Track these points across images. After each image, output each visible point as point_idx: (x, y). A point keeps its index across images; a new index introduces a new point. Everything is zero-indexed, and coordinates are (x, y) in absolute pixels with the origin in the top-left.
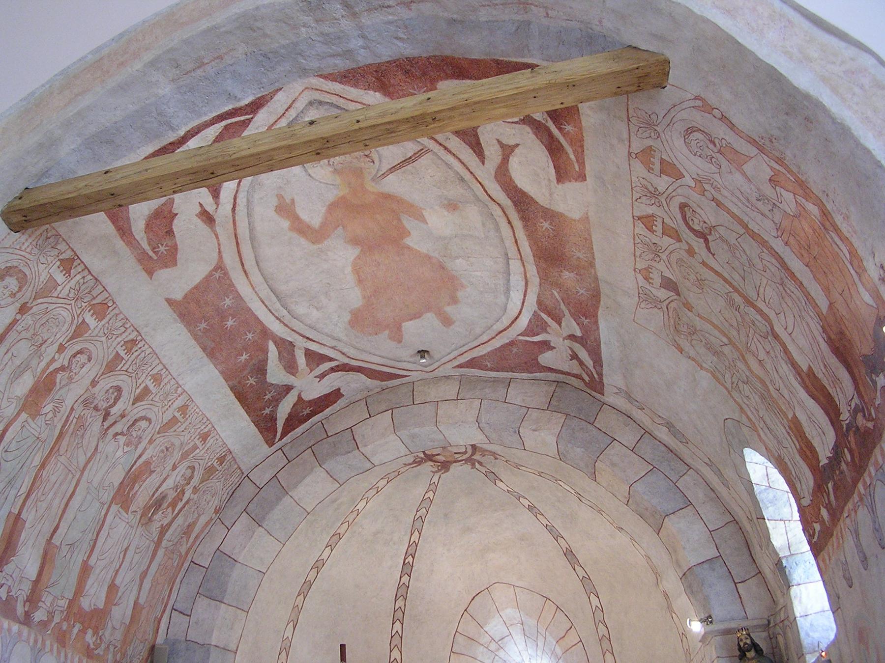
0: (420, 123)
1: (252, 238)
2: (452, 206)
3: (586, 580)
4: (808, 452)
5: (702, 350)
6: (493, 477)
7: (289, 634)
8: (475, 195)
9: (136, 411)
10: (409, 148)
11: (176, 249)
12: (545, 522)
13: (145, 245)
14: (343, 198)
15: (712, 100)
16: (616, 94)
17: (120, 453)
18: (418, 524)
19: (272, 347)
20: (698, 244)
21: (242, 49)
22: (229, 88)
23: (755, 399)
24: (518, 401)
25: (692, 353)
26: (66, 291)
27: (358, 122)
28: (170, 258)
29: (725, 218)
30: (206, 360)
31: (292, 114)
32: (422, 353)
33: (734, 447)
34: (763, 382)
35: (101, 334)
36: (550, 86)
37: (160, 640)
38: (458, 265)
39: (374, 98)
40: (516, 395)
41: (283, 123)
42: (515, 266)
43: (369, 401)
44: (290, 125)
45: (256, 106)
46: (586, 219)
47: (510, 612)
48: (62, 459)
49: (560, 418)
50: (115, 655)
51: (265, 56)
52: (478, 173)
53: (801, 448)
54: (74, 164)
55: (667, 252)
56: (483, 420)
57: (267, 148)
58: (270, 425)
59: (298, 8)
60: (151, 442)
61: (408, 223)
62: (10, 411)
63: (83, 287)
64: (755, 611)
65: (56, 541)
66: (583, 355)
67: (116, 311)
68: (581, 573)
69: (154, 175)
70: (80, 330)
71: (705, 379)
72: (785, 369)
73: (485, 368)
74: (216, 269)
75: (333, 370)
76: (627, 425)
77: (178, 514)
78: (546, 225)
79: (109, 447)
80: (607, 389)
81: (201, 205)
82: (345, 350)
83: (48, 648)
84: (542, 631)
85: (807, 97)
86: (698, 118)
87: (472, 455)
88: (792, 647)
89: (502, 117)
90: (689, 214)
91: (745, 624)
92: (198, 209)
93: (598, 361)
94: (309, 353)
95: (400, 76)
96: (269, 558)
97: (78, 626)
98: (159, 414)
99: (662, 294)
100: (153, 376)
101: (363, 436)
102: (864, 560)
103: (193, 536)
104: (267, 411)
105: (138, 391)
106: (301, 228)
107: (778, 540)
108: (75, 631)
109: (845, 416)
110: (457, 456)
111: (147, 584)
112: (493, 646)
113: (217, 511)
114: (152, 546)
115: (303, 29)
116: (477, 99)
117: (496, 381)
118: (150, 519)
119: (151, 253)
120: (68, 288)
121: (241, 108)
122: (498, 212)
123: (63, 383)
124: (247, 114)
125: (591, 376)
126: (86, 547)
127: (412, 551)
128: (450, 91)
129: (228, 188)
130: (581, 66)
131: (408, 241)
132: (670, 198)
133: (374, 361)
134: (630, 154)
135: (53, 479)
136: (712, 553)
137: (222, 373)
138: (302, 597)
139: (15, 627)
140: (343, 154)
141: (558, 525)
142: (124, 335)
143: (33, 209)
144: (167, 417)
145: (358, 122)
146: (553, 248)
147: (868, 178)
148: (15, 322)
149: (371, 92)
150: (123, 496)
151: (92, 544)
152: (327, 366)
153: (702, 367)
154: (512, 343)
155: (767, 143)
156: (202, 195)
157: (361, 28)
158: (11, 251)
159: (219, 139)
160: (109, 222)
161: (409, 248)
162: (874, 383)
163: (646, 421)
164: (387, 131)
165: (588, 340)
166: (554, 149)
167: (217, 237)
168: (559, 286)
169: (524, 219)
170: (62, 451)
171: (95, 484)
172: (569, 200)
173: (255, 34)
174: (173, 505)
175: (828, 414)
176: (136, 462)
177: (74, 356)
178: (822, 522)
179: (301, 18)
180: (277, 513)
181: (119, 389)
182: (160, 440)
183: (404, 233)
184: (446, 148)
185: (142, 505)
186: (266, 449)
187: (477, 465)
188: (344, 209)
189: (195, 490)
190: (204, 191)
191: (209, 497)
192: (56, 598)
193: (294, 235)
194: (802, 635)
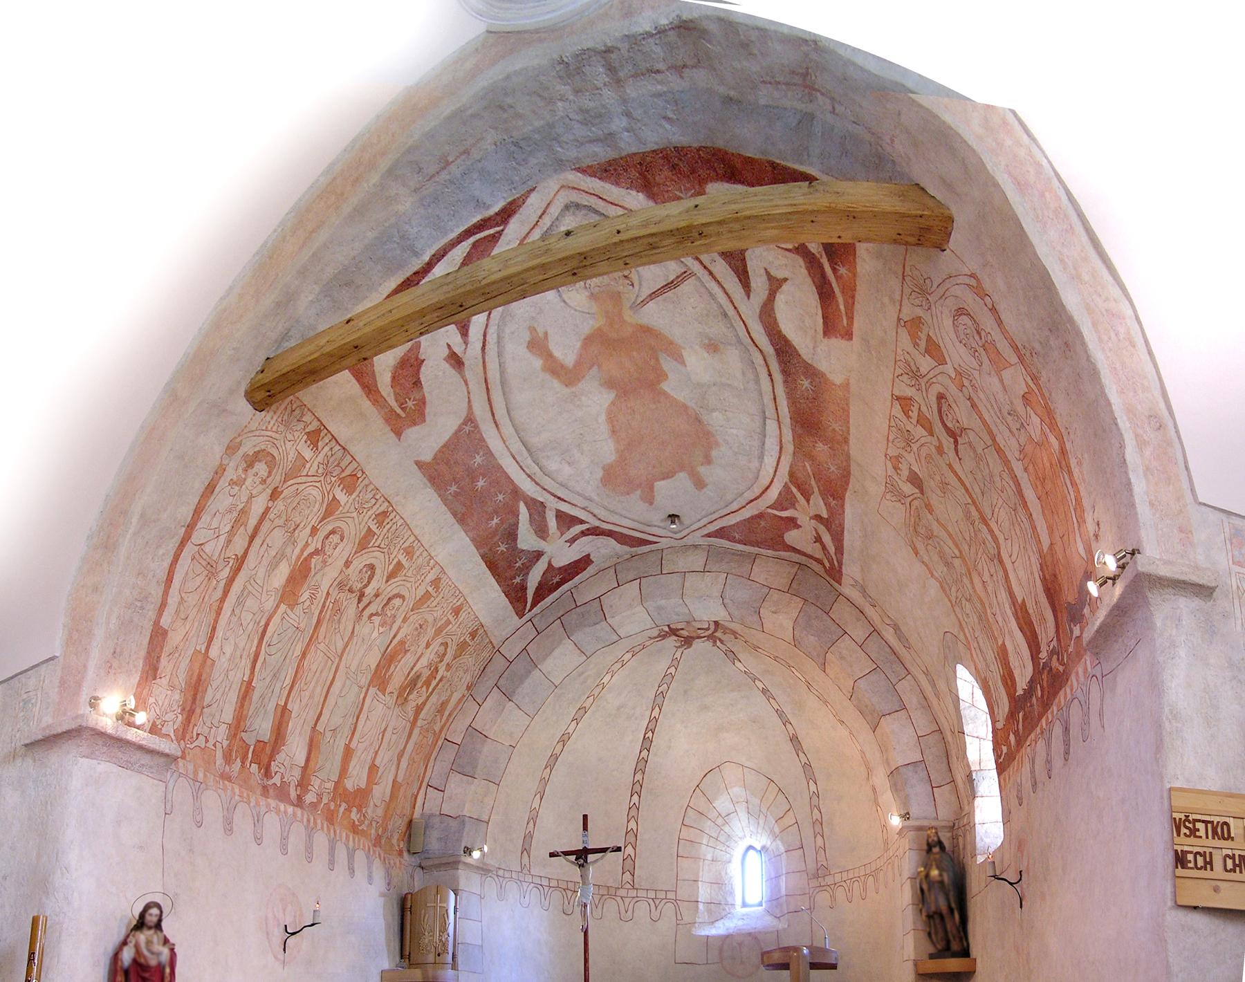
0: (686, 238)
1: (503, 383)
2: (713, 347)
3: (807, 766)
4: (1009, 680)
5: (936, 558)
6: (732, 656)
7: (536, 805)
8: (737, 336)
9: (389, 589)
10: (672, 269)
11: (424, 403)
12: (776, 707)
13: (392, 402)
14: (599, 329)
15: (987, 285)
16: (895, 241)
17: (375, 634)
18: (659, 700)
19: (523, 509)
20: (947, 443)
21: (491, 136)
22: (477, 193)
23: (974, 619)
25: (926, 558)
27: (619, 232)
28: (418, 415)
29: (975, 423)
30: (457, 526)
31: (547, 222)
32: (673, 518)
33: (950, 660)
34: (982, 603)
35: (352, 509)
36: (830, 210)
37: (417, 815)
38: (715, 420)
39: (636, 200)
40: (761, 573)
41: (536, 235)
42: (771, 426)
43: (618, 567)
44: (544, 237)
45: (506, 214)
46: (846, 386)
47: (737, 791)
48: (322, 646)
49: (798, 603)
50: (377, 831)
51: (516, 144)
52: (742, 309)
54: (317, 320)
55: (919, 444)
56: (727, 594)
57: (519, 268)
59: (554, 73)
60: (405, 620)
61: (667, 364)
62: (269, 605)
64: (945, 814)
65: (320, 728)
66: (827, 538)
67: (366, 482)
68: (804, 760)
69: (398, 316)
71: (933, 589)
72: (1003, 596)
73: (732, 540)
74: (465, 423)
75: (583, 534)
76: (858, 620)
78: (806, 383)
79: (365, 629)
80: (844, 580)
81: (449, 346)
82: (596, 512)
83: (319, 826)
84: (764, 810)
85: (1070, 320)
86: (971, 301)
88: (969, 847)
89: (773, 240)
90: (944, 408)
91: (934, 823)
93: (840, 549)
94: (560, 515)
95: (667, 173)
96: (518, 731)
97: (344, 805)
98: (413, 591)
99: (908, 489)
100: (405, 550)
102: (1035, 785)
103: (447, 713)
104: (518, 580)
105: (391, 567)
106: (554, 368)
107: (972, 755)
108: (342, 809)
109: (1043, 655)
111: (404, 764)
112: (720, 821)
113: (468, 688)
115: (560, 104)
116: (747, 213)
117: (742, 554)
119: (399, 411)
120: (316, 463)
121: (489, 219)
122: (759, 360)
123: (318, 567)
124: (497, 225)
125: (831, 562)
126: (347, 731)
128: (721, 196)
129: (478, 321)
130: (864, 193)
131: (665, 386)
132: (930, 384)
133: (624, 524)
134: (899, 319)
135: (314, 668)
136: (918, 757)
137: (473, 540)
139: (290, 809)
140: (600, 275)
141: (787, 710)
142: (375, 508)
143: (276, 381)
145: (619, 232)
146: (811, 414)
147: (1104, 431)
148: (267, 510)
149: (634, 193)
150: (380, 678)
152: (578, 529)
153: (932, 576)
154: (761, 516)
155: (1028, 354)
156: (449, 335)
157: (625, 101)
158: (257, 433)
159: (467, 261)
160: (354, 381)
161: (665, 394)
162: (1072, 632)
163: (877, 620)
164: (650, 246)
165: (832, 524)
166: (825, 293)
167: (466, 384)
168: (812, 458)
169: (785, 372)
171: (353, 668)
172: (831, 359)
173: (505, 116)
175: (1030, 647)
177: (327, 537)
178: (1009, 747)
179: (558, 87)
181: (372, 567)
183: (661, 376)
184: (711, 273)
185: (397, 686)
186: (515, 621)
188: (601, 342)
189: (449, 667)
190: (452, 328)
191: (461, 673)
192: (322, 782)
193: (548, 376)
194: (978, 839)
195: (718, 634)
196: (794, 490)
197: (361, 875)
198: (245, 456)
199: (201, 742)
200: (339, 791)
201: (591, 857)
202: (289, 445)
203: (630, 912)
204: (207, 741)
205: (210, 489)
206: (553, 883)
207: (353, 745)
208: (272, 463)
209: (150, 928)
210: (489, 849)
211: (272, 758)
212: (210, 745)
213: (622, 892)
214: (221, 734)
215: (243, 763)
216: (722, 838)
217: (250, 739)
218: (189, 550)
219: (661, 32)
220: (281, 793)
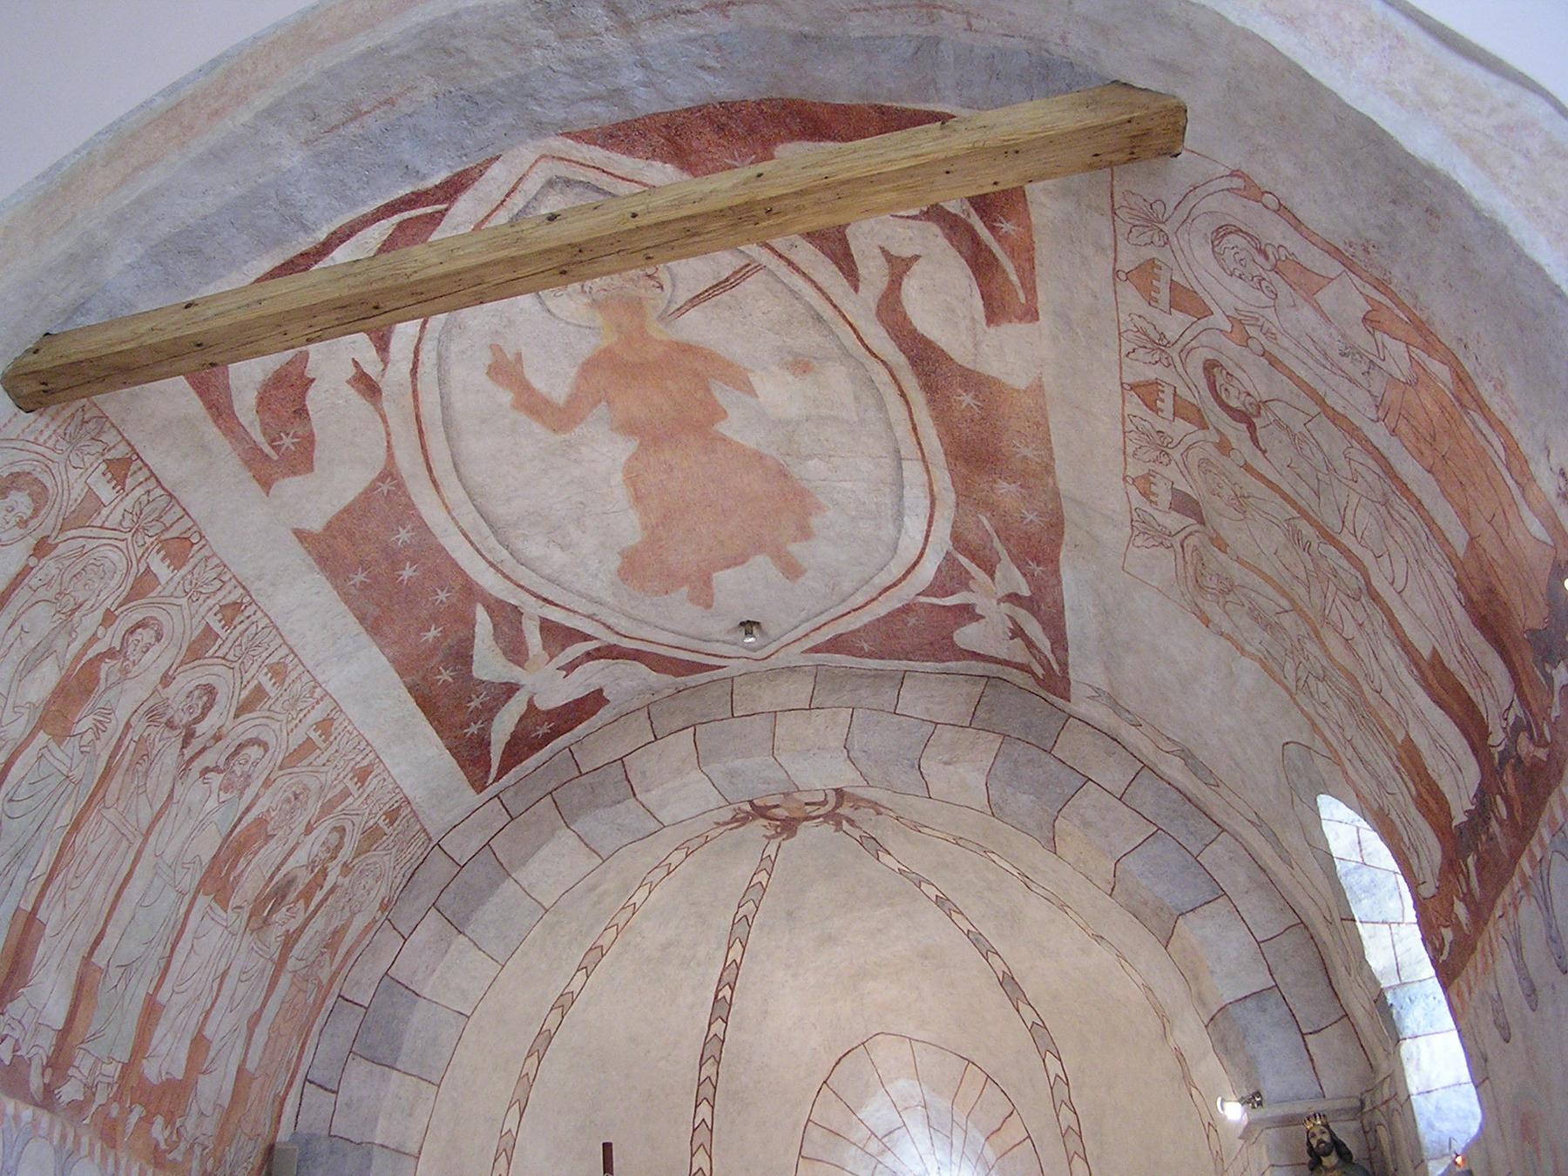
0: (744, 218)
1: (447, 423)
2: (801, 365)
3: (1038, 1030)
4: (1431, 801)
5: (1244, 622)
6: (874, 846)
7: (511, 1124)
8: (842, 346)
9: (240, 729)
10: (725, 262)
11: (312, 442)
12: (966, 926)
13: (257, 435)
14: (608, 350)
15: (1262, 177)
16: (1091, 166)
17: (212, 803)
18: (741, 929)
19: (481, 615)
20: (1236, 433)
21: (428, 86)
22: (407, 157)
23: (1338, 708)
24: (918, 712)
25: (1226, 627)
26: (117, 516)
27: (634, 216)
28: (302, 458)
29: (1285, 386)
30: (365, 638)
31: (518, 201)
32: (748, 626)
33: (1301, 794)
34: (1351, 677)
35: (179, 592)
36: (975, 152)
37: (283, 1135)
38: (812, 471)
39: (662, 173)
40: (914, 701)
41: (502, 218)
42: (913, 471)
43: (653, 710)
44: (513, 222)
45: (453, 188)
46: (1038, 389)
47: (904, 1086)
48: (110, 814)
49: (991, 742)
50: (203, 1162)
51: (469, 99)
52: (847, 307)
53: (1420, 794)
54: (132, 291)
55: (1182, 448)
56: (856, 745)
57: (472, 262)
58: (478, 753)
59: (527, 14)
60: (267, 783)
61: (723, 395)
62: (17, 729)
63: (147, 510)
64: (1338, 1083)
65: (100, 959)
66: (1034, 629)
67: (206, 552)
68: (1030, 1017)
69: (272, 310)
70: (142, 585)
71: (1249, 673)
72: (1391, 654)
73: (860, 653)
74: (382, 477)
75: (590, 656)
76: (1110, 754)
77: (315, 912)
78: (967, 399)
79: (193, 792)
80: (1076, 690)
81: (356, 363)
82: (611, 621)
83: (85, 1150)
84: (961, 1119)
85: (1430, 172)
86: (1237, 210)
87: (836, 807)
88: (1404, 1147)
89: (890, 207)
90: (1220, 380)
91: (1319, 1106)
92: (351, 371)
93: (1059, 641)
94: (547, 627)
95: (709, 134)
96: (476, 989)
97: (138, 1111)
98: (282, 735)
99: (1174, 521)
100: (271, 668)
101: (644, 773)
102: (1532, 993)
103: (342, 950)
104: (474, 729)
105: (245, 693)
106: (532, 404)
107: (1378, 958)
108: (134, 1118)
109: (1497, 738)
110: (809, 808)
111: (260, 1037)
112: (874, 1146)
113: (384, 907)
114: (270, 969)
115: (537, 52)
116: (846, 175)
117: (878, 675)
118: (266, 920)
119: (267, 449)
120: (120, 510)
121: (426, 192)
122: (882, 376)
123: (112, 679)
124: (437, 202)
125: (1047, 667)
126: (152, 970)
127: (729, 978)
128: (797, 161)
129: (405, 333)
130: (1029, 117)
131: (723, 428)
132: (1186, 351)
133: (662, 640)
134: (1116, 273)
135: (94, 849)
136: (1262, 980)
137: (393, 661)
138: (534, 1059)
139: (27, 1113)
140: (608, 273)
141: (988, 931)
142: (220, 595)
143: (58, 371)
144: (297, 739)
145: (634, 216)
146: (980, 441)
147: (1537, 315)
148: (26, 571)
149: (658, 164)
150: (218, 879)
151: (162, 965)
152: (579, 649)
153: (1243, 652)
154: (907, 609)
155: (1360, 253)
156: (358, 346)
157: (639, 49)
158: (19, 445)
159: (387, 246)
160: (194, 395)
161: (724, 439)
162: (1549, 679)
163: (1145, 747)
164: (686, 233)
165: (1043, 603)
166: (981, 264)
167: (385, 421)
168: (990, 507)
169: (929, 388)
170: (110, 799)
171: (168, 858)
172: (1008, 355)
173: (451, 61)
174: (307, 895)
175: (1466, 734)
176: (240, 819)
177: (132, 631)
178: (1456, 927)
179: (534, 31)
180: (490, 911)
181: (210, 691)
182: (283, 781)
183: (716, 413)
184: (790, 263)
185: (251, 895)
186: (470, 797)
187: (845, 825)
188: (609, 371)
189: (346, 869)
190: (362, 339)
191: (370, 881)
192: (99, 1061)
193: (522, 417)
194: (1422, 1126)
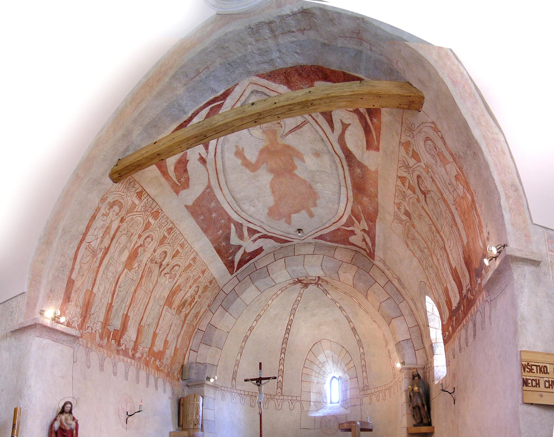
0: (305, 106)
1: (224, 170)
2: (317, 154)
3: (359, 341)
4: (449, 302)
5: (416, 248)
6: (326, 292)
7: (238, 358)
8: (328, 149)
9: (173, 262)
10: (299, 120)
11: (189, 179)
12: (345, 315)
13: (174, 179)
14: (267, 146)
15: (439, 127)
16: (398, 107)
17: (167, 282)
18: (293, 311)
19: (233, 227)
20: (422, 197)
21: (219, 61)
22: (212, 86)
23: (433, 275)
25: (412, 249)
27: (275, 103)
28: (186, 184)
29: (434, 188)
30: (203, 234)
31: (243, 99)
32: (299, 230)
33: (423, 294)
34: (437, 268)
35: (157, 227)
36: (369, 94)
37: (185, 363)
38: (318, 187)
39: (283, 89)
40: (339, 255)
41: (239, 104)
42: (343, 189)
43: (275, 252)
44: (242, 105)
45: (225, 95)
46: (376, 172)
47: (328, 352)
48: (143, 288)
49: (355, 268)
50: (168, 370)
51: (230, 64)
52: (330, 137)
54: (141, 142)
55: (409, 197)
56: (324, 265)
57: (231, 119)
59: (247, 33)
60: (180, 276)
61: (297, 162)
62: (120, 269)
64: (421, 362)
65: (142, 324)
66: (368, 240)
67: (163, 214)
68: (358, 338)
69: (177, 141)
71: (415, 262)
72: (446, 265)
73: (326, 240)
74: (207, 188)
75: (260, 237)
76: (382, 276)
78: (359, 171)
79: (162, 280)
80: (376, 258)
81: (200, 154)
82: (265, 228)
83: (142, 368)
84: (340, 361)
85: (476, 142)
86: (432, 134)
88: (431, 377)
89: (344, 107)
90: (420, 182)
91: (416, 366)
93: (374, 244)
94: (249, 229)
95: (297, 77)
96: (231, 325)
97: (153, 358)
98: (184, 263)
99: (404, 217)
100: (180, 245)
102: (460, 349)
103: (199, 317)
104: (230, 258)
105: (174, 252)
106: (247, 164)
107: (433, 336)
108: (152, 360)
109: (464, 291)
111: (180, 340)
112: (320, 365)
113: (208, 306)
115: (249, 46)
116: (333, 95)
117: (330, 247)
119: (177, 183)
120: (141, 206)
121: (218, 97)
122: (338, 160)
123: (142, 252)
124: (221, 100)
125: (370, 250)
126: (154, 325)
128: (321, 87)
129: (213, 143)
130: (384, 86)
131: (296, 172)
132: (414, 171)
133: (278, 233)
134: (400, 142)
135: (140, 297)
136: (409, 337)
137: (210, 240)
139: (129, 360)
140: (267, 122)
141: (350, 316)
142: (167, 226)
143: (123, 170)
145: (275, 103)
146: (361, 184)
147: (491, 192)
148: (119, 227)
149: (282, 86)
150: (169, 302)
152: (257, 235)
153: (415, 256)
154: (338, 230)
155: (457, 158)
156: (200, 149)
157: (278, 45)
158: (115, 193)
159: (208, 116)
160: (158, 170)
161: (296, 175)
162: (477, 281)
163: (390, 276)
164: (289, 110)
165: (370, 233)
166: (367, 131)
167: (208, 171)
168: (361, 204)
169: (349, 166)
171: (157, 297)
172: (370, 160)
173: (225, 51)
175: (458, 288)
177: (145, 239)
178: (449, 332)
179: (248, 39)
181: (165, 252)
183: (294, 167)
184: (316, 122)
185: (177, 305)
186: (229, 276)
188: (267, 152)
189: (200, 297)
190: (201, 146)
191: (205, 299)
192: (144, 348)
193: (244, 167)
194: (435, 373)
195: (320, 282)
196: (353, 218)
197: (160, 390)
198: (109, 203)
199: (89, 330)
200: (151, 352)
201: (263, 382)
202: (129, 198)
203: (280, 406)
204: (92, 330)
205: (94, 218)
206: (246, 393)
207: (157, 332)
208: (121, 206)
209: (67, 413)
210: (218, 378)
211: (121, 337)
212: (93, 331)
213: (277, 397)
214: (98, 327)
215: (108, 339)
216: (321, 373)
217: (111, 329)
218: (84, 245)
219: (294, 14)
220: (125, 353)
